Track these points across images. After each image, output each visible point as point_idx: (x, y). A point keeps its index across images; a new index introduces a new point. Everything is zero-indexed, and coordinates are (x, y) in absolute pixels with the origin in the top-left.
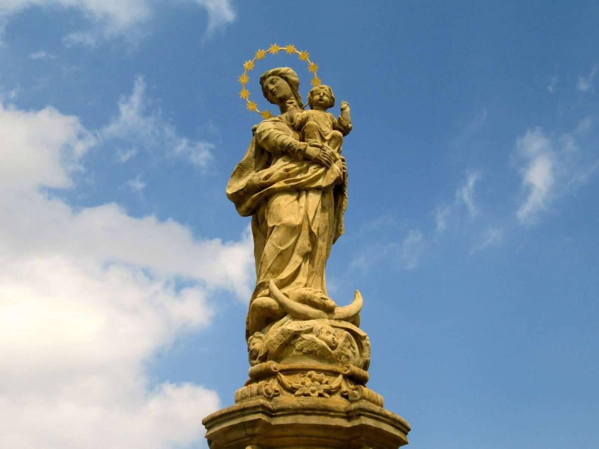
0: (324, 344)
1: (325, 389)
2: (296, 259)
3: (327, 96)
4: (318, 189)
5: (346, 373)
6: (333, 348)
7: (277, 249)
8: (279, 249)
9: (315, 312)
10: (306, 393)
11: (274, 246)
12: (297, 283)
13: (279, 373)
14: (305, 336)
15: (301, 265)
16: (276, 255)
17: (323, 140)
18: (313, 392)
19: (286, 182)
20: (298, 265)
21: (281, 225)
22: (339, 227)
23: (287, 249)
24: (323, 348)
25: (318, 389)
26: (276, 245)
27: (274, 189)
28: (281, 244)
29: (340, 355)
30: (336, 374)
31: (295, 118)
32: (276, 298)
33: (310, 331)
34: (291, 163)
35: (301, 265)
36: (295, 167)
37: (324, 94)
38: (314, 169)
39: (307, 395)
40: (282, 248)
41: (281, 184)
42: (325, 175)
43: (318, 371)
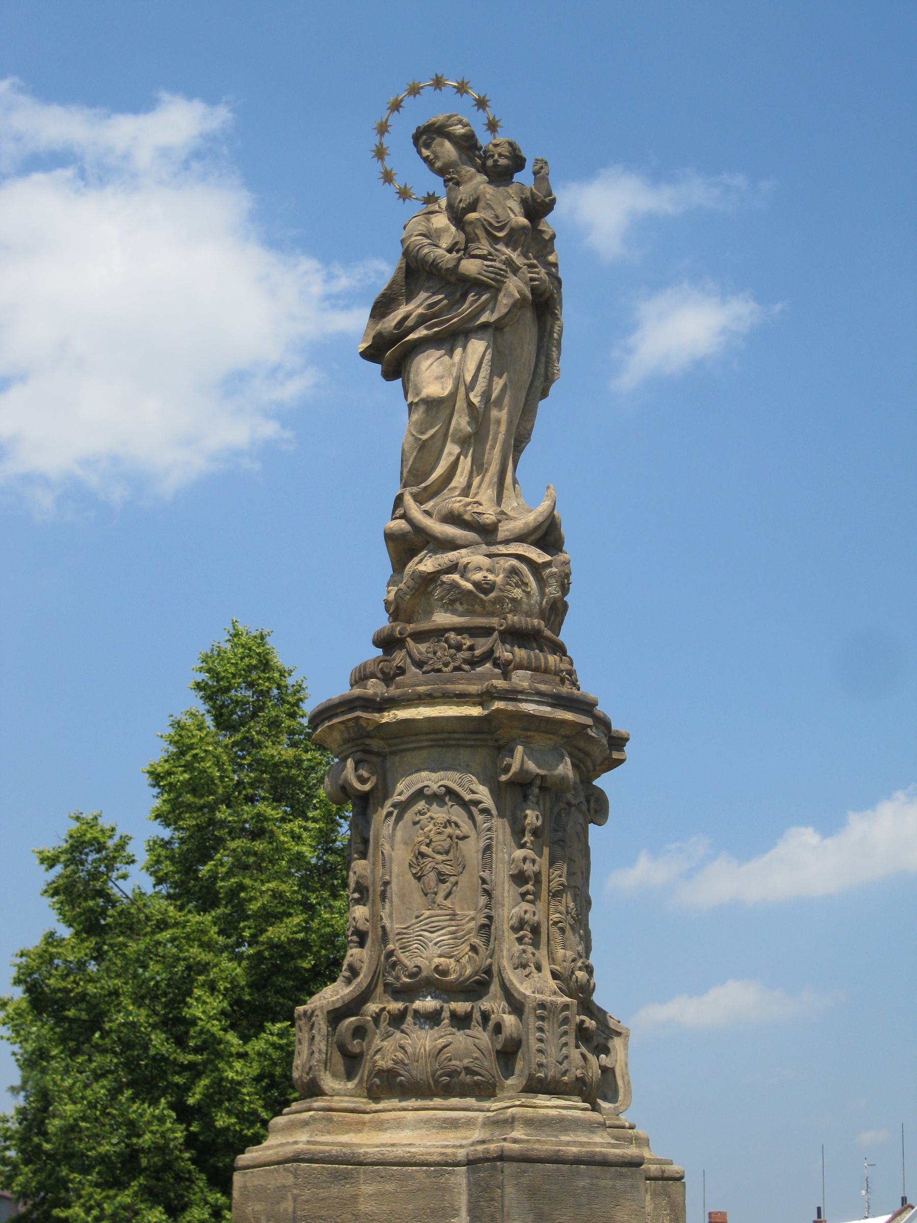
0: (470, 586)
1: (463, 659)
2: (451, 449)
3: (506, 157)
4: (485, 326)
5: (502, 628)
6: (486, 592)
7: (417, 439)
8: (420, 439)
9: (466, 536)
10: (436, 667)
11: (413, 435)
12: (449, 490)
13: (408, 639)
14: (446, 578)
15: (458, 459)
16: (417, 449)
17: (495, 240)
18: (446, 665)
19: (427, 328)
20: (453, 458)
21: (419, 401)
22: (550, 369)
23: (432, 437)
24: (470, 592)
25: (454, 660)
26: (414, 433)
27: (409, 340)
28: (423, 433)
29: (499, 600)
30: (487, 631)
31: (456, 205)
32: (410, 521)
33: (452, 568)
34: (434, 294)
35: (458, 459)
36: (441, 300)
37: (500, 155)
38: (474, 296)
39: (439, 671)
40: (424, 437)
41: (421, 332)
42: (495, 304)
43: (459, 630)
